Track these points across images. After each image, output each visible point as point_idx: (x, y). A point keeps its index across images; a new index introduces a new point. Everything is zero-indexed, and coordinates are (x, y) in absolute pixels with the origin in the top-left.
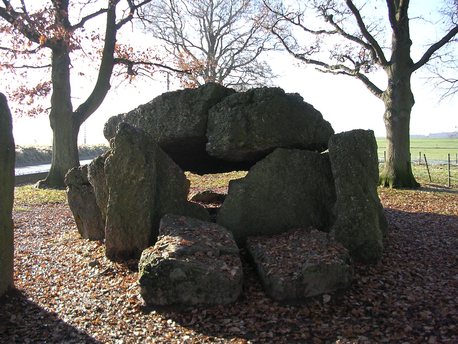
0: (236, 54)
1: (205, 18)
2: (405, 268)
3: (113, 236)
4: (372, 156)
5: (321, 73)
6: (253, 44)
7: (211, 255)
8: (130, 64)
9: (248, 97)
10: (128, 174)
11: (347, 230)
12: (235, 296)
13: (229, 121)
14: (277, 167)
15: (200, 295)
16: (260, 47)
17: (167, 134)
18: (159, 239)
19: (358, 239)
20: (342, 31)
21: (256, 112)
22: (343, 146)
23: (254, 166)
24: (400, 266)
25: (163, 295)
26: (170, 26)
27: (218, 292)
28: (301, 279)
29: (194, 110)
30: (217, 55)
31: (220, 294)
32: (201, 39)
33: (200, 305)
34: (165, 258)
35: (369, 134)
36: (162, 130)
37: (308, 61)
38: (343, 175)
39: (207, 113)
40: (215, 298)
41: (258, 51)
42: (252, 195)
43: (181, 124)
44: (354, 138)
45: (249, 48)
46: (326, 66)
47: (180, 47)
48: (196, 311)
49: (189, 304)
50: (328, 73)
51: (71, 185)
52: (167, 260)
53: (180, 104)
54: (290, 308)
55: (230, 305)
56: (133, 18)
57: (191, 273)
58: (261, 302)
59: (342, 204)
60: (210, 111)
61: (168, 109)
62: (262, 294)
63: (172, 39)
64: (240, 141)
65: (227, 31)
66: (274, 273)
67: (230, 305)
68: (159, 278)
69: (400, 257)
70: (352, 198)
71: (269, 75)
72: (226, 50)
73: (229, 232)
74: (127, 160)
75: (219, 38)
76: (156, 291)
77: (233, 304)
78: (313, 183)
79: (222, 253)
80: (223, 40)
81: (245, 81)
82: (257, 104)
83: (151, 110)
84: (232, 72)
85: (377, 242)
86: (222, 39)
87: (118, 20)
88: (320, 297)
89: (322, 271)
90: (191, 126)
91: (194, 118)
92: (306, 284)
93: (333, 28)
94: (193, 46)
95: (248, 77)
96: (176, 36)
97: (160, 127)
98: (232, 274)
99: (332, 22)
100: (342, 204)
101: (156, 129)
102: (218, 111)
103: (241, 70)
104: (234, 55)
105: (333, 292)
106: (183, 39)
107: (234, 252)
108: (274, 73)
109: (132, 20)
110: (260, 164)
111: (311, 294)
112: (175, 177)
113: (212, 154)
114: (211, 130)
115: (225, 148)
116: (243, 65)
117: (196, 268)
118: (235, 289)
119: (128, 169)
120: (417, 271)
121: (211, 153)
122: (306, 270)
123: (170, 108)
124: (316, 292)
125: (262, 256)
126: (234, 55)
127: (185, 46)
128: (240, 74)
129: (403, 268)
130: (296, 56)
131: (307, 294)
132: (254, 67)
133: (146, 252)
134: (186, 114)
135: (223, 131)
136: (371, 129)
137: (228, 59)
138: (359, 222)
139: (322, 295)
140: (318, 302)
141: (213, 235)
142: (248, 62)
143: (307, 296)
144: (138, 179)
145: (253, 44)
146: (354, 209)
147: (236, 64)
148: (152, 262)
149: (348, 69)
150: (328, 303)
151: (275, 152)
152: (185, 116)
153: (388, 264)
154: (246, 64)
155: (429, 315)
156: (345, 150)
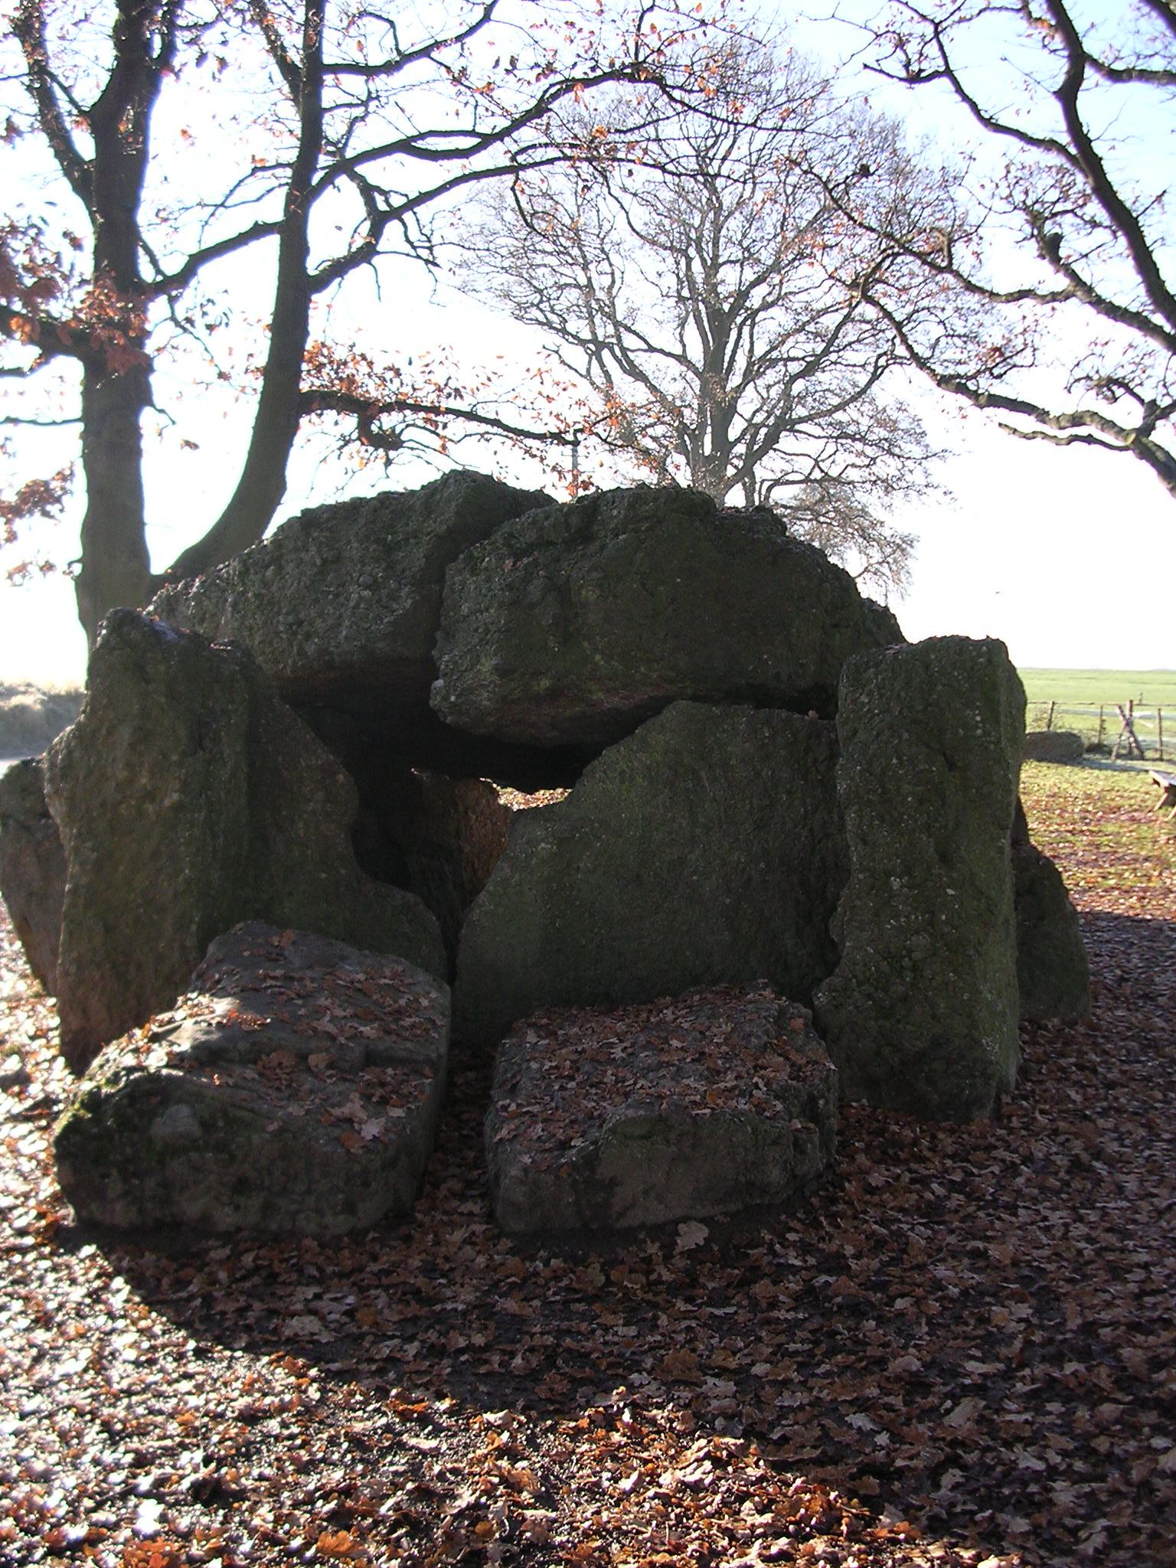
0: (801, 375)
1: (692, 252)
2: (1068, 1140)
3: (81, 991)
4: (986, 733)
5: (1015, 438)
6: (858, 341)
7: (322, 1066)
8: (366, 410)
9: (574, 520)
10: (131, 781)
11: (869, 996)
12: (369, 1211)
13: (501, 605)
14: (670, 768)
15: (242, 1200)
16: (885, 353)
17: (311, 648)
18: (179, 1003)
19: (909, 1028)
20: (1089, 290)
21: (595, 575)
22: (882, 696)
23: (596, 762)
24: (1055, 1132)
25: (126, 1194)
26: (572, 281)
27: (309, 1192)
28: (590, 1161)
29: (399, 568)
30: (735, 380)
31: (311, 1200)
32: (682, 325)
33: (245, 1234)
34: (152, 1070)
35: (980, 655)
36: (295, 634)
37: (982, 400)
38: (869, 800)
39: (441, 579)
40: (298, 1212)
41: (876, 368)
42: (582, 865)
43: (354, 614)
44: (927, 667)
45: (849, 356)
46: (1042, 415)
47: (606, 354)
48: (224, 1253)
49: (204, 1227)
50: (1039, 440)
51: (9, 817)
52: (155, 1078)
53: (356, 545)
54: (547, 1263)
55: (346, 1239)
56: (379, 253)
57: (221, 1124)
58: (458, 1235)
59: (858, 903)
60: (450, 570)
61: (315, 565)
62: (476, 1209)
63: (575, 325)
64: (537, 674)
65: (770, 299)
66: (515, 1137)
67: (346, 1239)
68: (117, 1137)
69: (1078, 1098)
70: (895, 883)
71: (917, 452)
72: (768, 362)
73: (440, 989)
74: (125, 734)
75: (743, 323)
76: (104, 1176)
77: (357, 1236)
78: (795, 827)
79: (371, 1058)
80: (755, 330)
81: (834, 472)
82: (603, 547)
83: (267, 567)
84: (786, 441)
85: (978, 1042)
86: (752, 326)
87: (313, 265)
88: (665, 1233)
89: (673, 1136)
90: (381, 620)
91: (394, 597)
92: (613, 1183)
93: (1061, 283)
94: (651, 349)
95: (843, 458)
96: (591, 317)
97: (291, 625)
98: (363, 1134)
99: (1056, 260)
100: (858, 903)
101: (277, 633)
102: (474, 571)
103: (818, 431)
104: (794, 378)
105: (725, 1214)
106: (617, 324)
107: (421, 1058)
108: (935, 442)
109: (376, 260)
110: (615, 757)
111: (634, 1218)
112: (320, 795)
113: (449, 720)
114: (449, 635)
115: (484, 699)
116: (822, 414)
117: (240, 1108)
118: (366, 1184)
119: (129, 765)
120: (1098, 1155)
121: (445, 717)
122: (613, 1131)
123: (324, 561)
124: (658, 1213)
125: (514, 1076)
126: (794, 378)
127: (624, 350)
128: (813, 447)
129: (1061, 1139)
130: (943, 381)
131: (622, 1215)
132: (865, 422)
133: (111, 1051)
134: (369, 580)
135: (482, 640)
136: (994, 637)
137: (774, 392)
138: (914, 968)
139: (676, 1222)
140: (653, 1249)
141: (370, 997)
142: (841, 407)
143: (623, 1223)
144: (162, 801)
145: (858, 341)
146: (897, 921)
147: (800, 411)
148: (109, 1082)
149: (1114, 425)
150: (689, 1254)
151: (669, 714)
152: (368, 587)
153: (1015, 1122)
154: (837, 408)
155: (1020, 1320)
156: (888, 711)
